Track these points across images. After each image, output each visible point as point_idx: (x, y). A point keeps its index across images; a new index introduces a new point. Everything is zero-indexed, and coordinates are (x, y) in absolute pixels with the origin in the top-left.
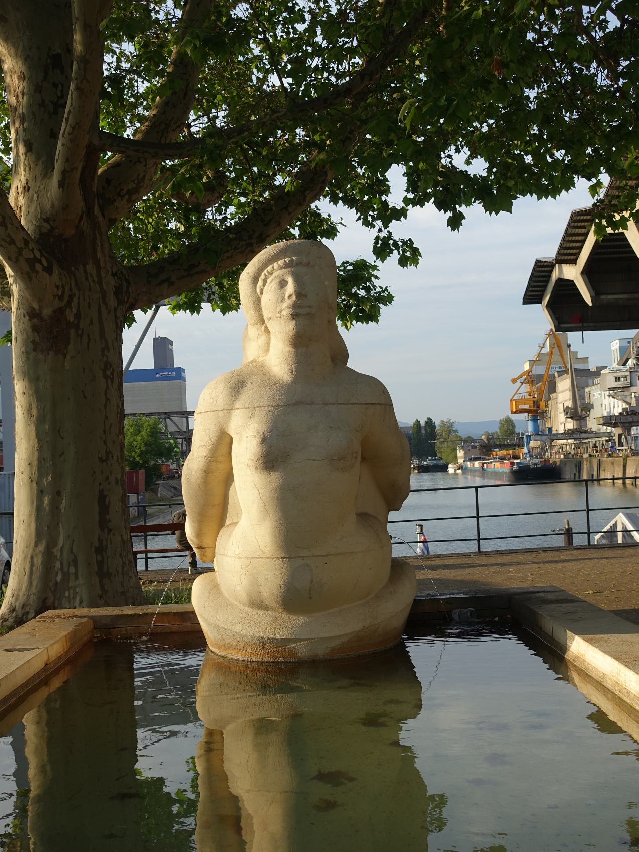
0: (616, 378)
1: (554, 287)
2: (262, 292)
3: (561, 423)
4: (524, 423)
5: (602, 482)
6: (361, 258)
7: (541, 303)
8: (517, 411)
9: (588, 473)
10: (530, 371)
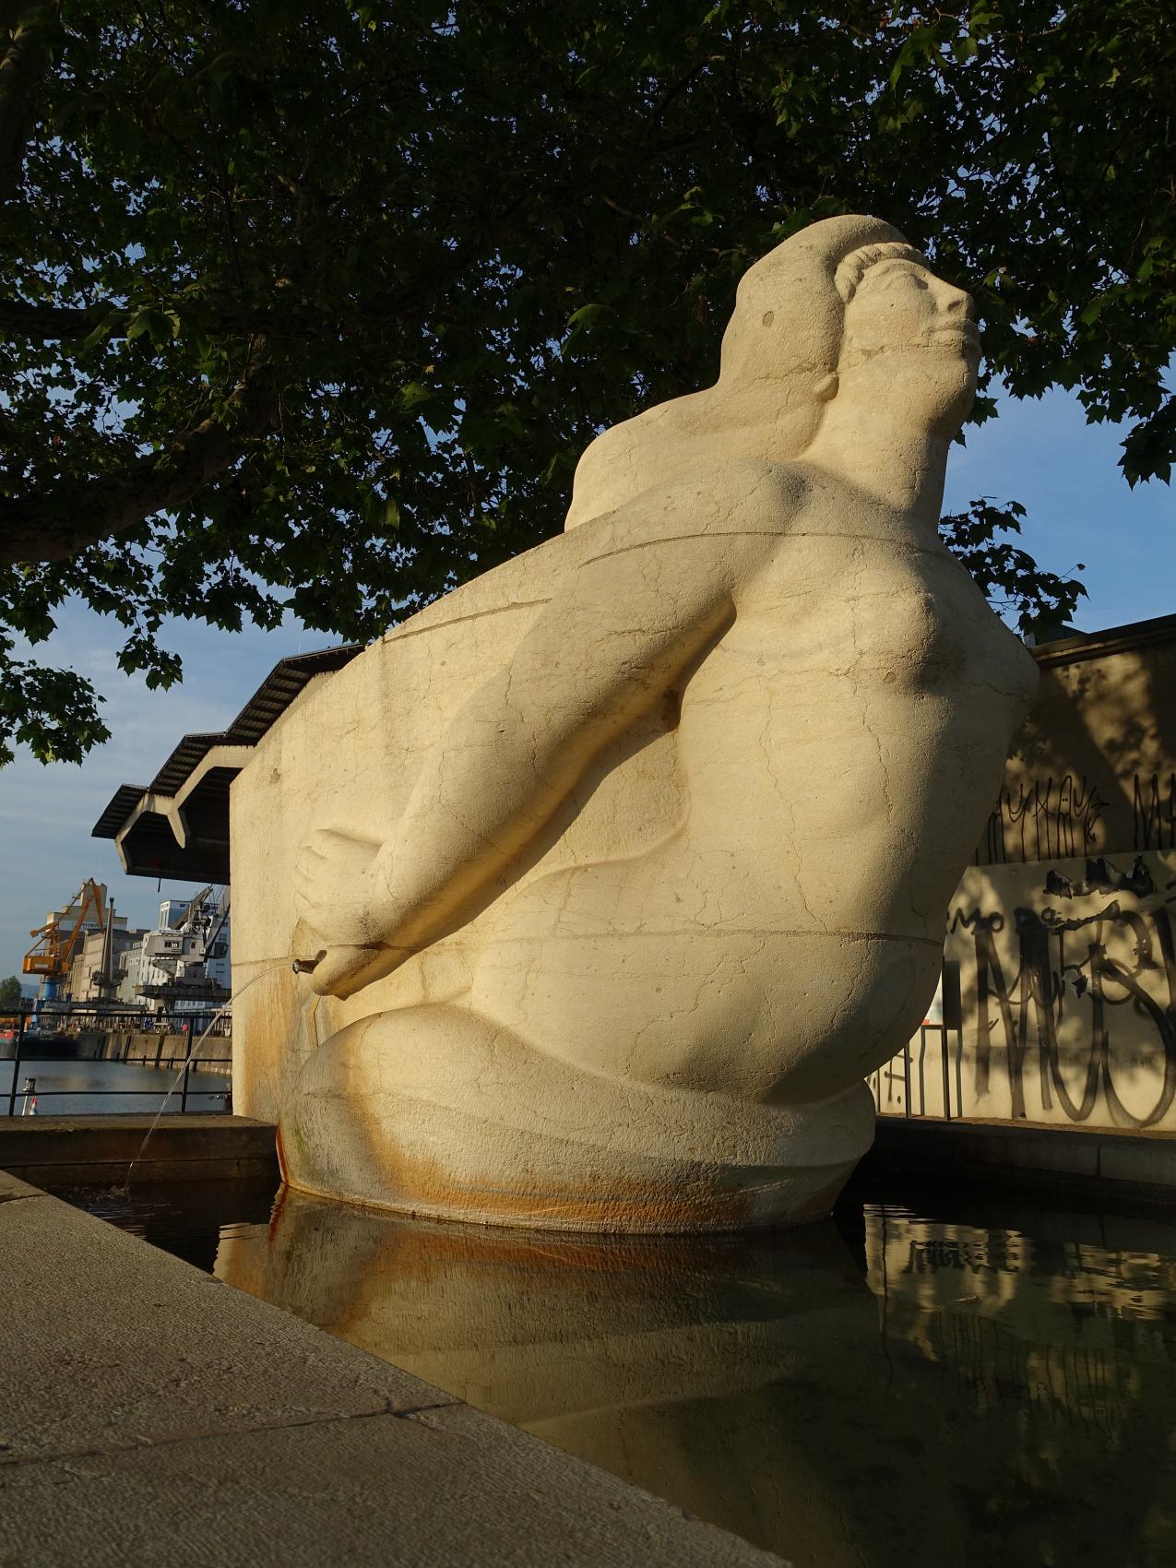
0: (166, 943)
1: (137, 822)
2: (852, 293)
3: (84, 989)
4: (36, 986)
5: (128, 1062)
6: (71, 670)
7: (115, 838)
8: (31, 970)
9: (114, 1052)
10: (53, 926)
